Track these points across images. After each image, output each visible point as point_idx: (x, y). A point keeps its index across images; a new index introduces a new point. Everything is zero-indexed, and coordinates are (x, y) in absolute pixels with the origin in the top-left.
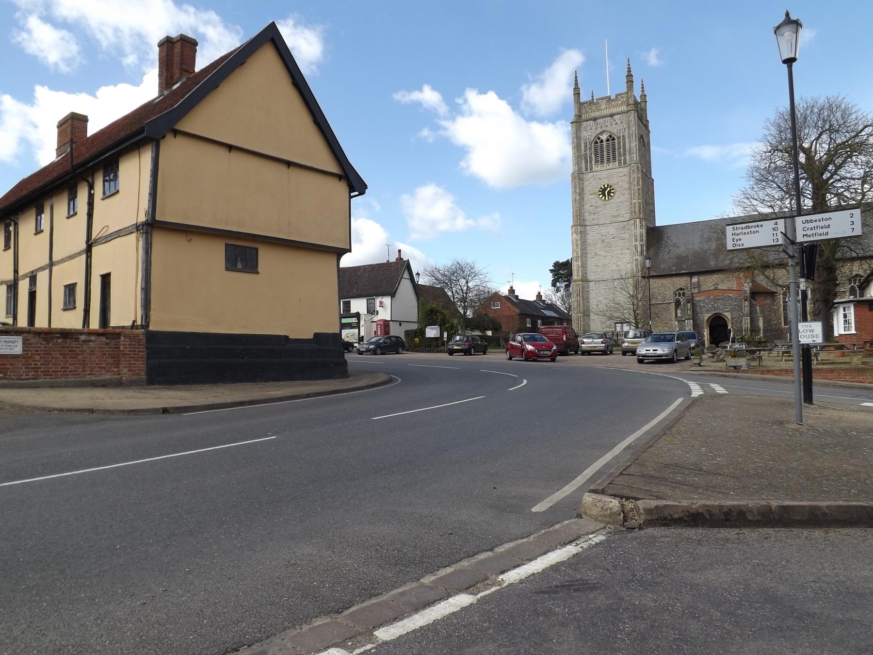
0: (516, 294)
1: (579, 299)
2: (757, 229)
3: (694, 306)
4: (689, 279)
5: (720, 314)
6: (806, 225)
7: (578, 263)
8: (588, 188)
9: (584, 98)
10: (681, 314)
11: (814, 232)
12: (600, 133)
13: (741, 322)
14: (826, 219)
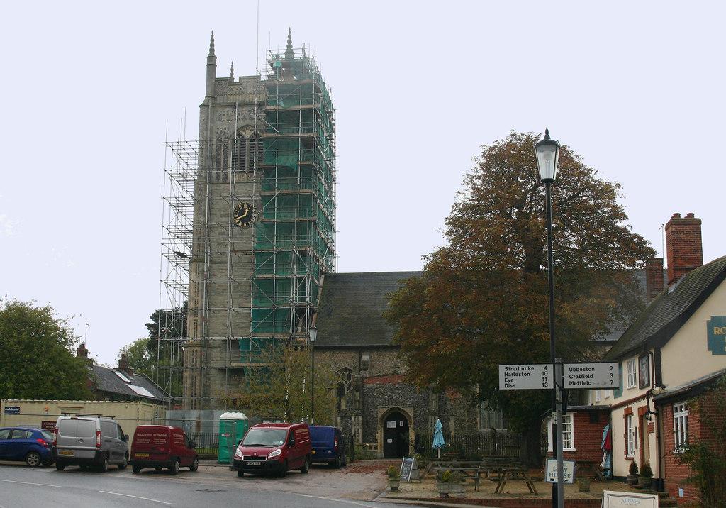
0: (89, 356)
1: (194, 374)
2: (528, 371)
3: (363, 395)
4: (357, 355)
5: (400, 409)
6: (572, 373)
7: (196, 318)
8: (218, 206)
9: (222, 72)
10: (346, 406)
11: (579, 380)
12: (243, 127)
13: (427, 421)
14: (590, 369)
